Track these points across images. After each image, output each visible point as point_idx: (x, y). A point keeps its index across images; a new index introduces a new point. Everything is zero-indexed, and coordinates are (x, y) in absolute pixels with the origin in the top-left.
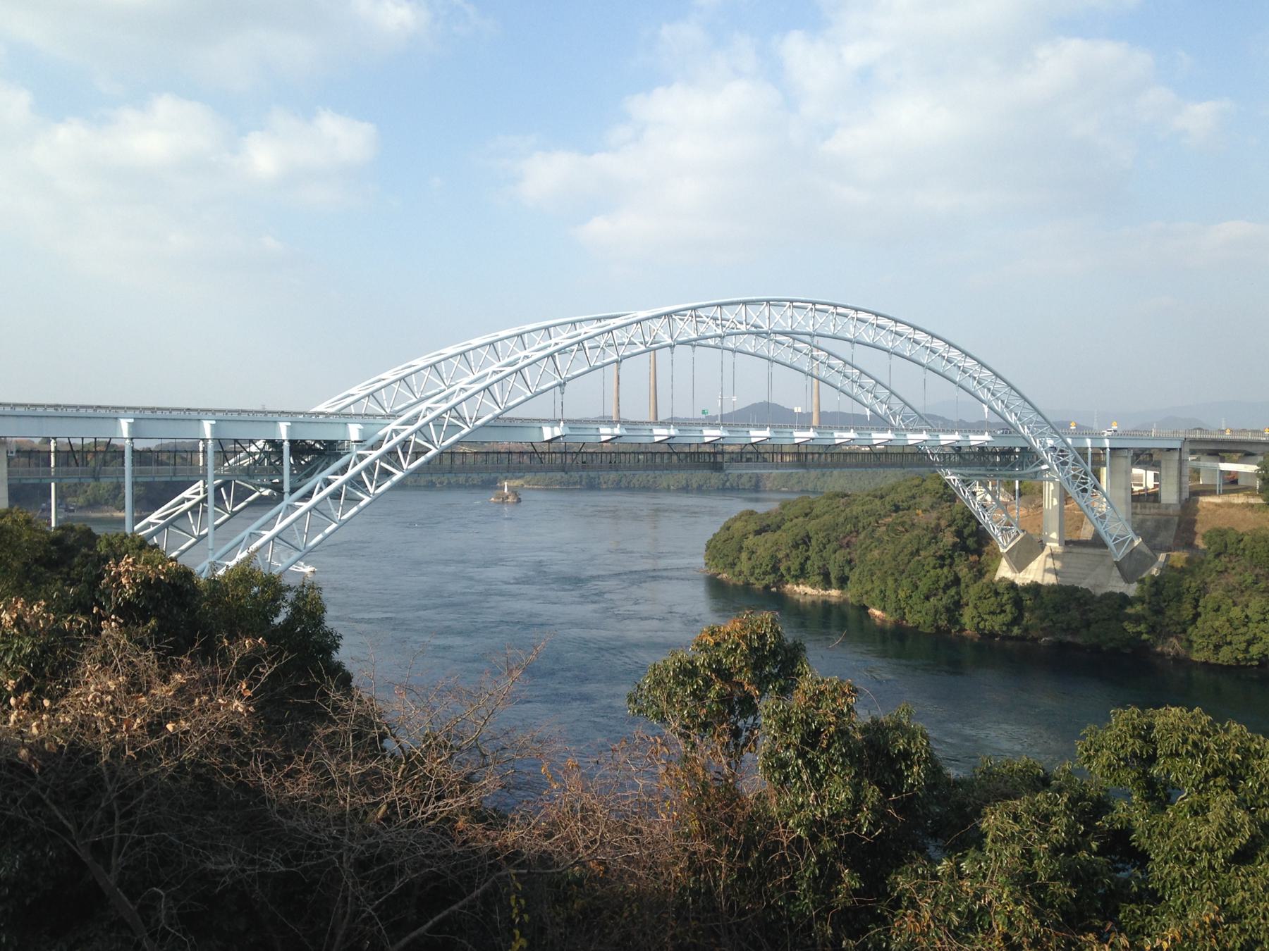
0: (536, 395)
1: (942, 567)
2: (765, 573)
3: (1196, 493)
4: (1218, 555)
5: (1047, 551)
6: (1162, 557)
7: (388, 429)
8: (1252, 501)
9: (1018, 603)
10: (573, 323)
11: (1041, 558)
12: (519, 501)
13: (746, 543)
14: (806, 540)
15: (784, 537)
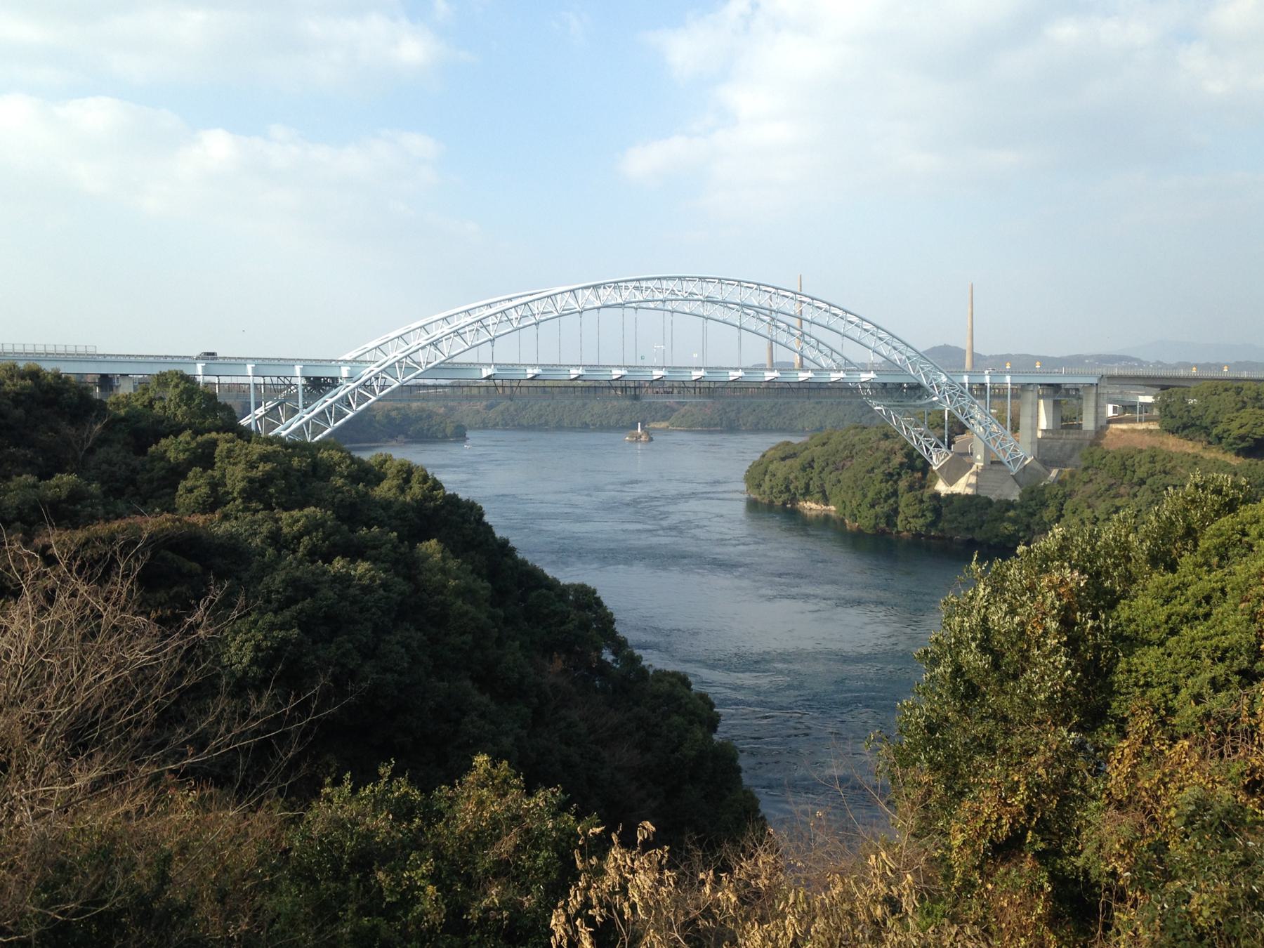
1: (887, 481)
2: (781, 492)
4: (1086, 469)
7: (368, 370)
9: (937, 511)
12: (651, 440)
15: (796, 463)
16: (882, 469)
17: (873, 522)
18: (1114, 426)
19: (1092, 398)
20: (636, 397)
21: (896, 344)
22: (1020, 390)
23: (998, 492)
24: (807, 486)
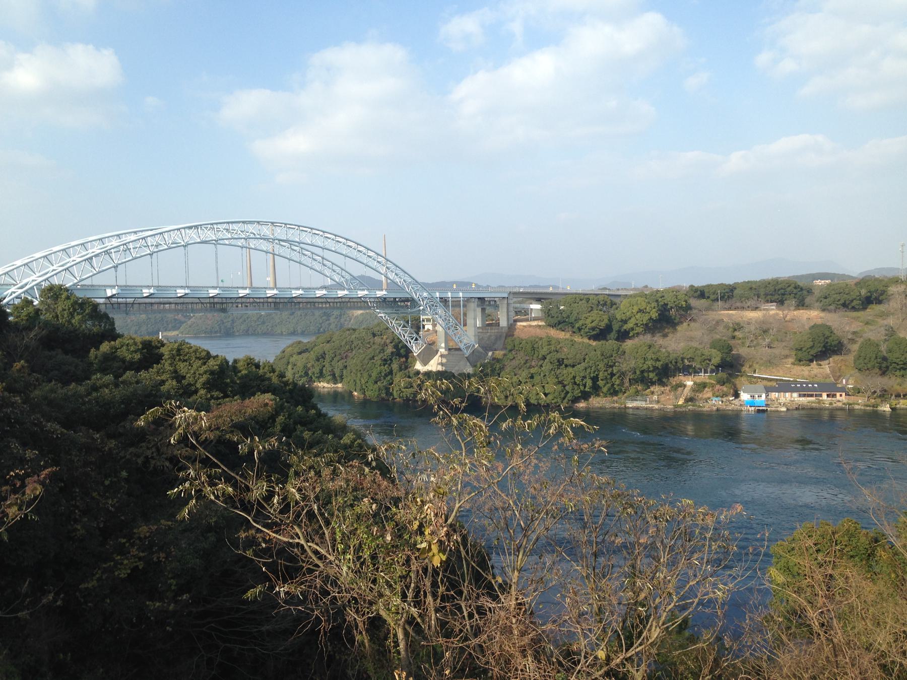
0: (99, 272)
3: (515, 321)
5: (439, 354)
6: (490, 354)
7: (10, 291)
8: (540, 324)
10: (118, 235)
11: (437, 357)
13: (292, 360)
14: (323, 356)
15: (312, 355)
16: (380, 356)
17: (377, 393)
18: (519, 324)
19: (505, 306)
20: (224, 310)
21: (398, 271)
22: (468, 300)
23: (457, 368)
24: (321, 371)
